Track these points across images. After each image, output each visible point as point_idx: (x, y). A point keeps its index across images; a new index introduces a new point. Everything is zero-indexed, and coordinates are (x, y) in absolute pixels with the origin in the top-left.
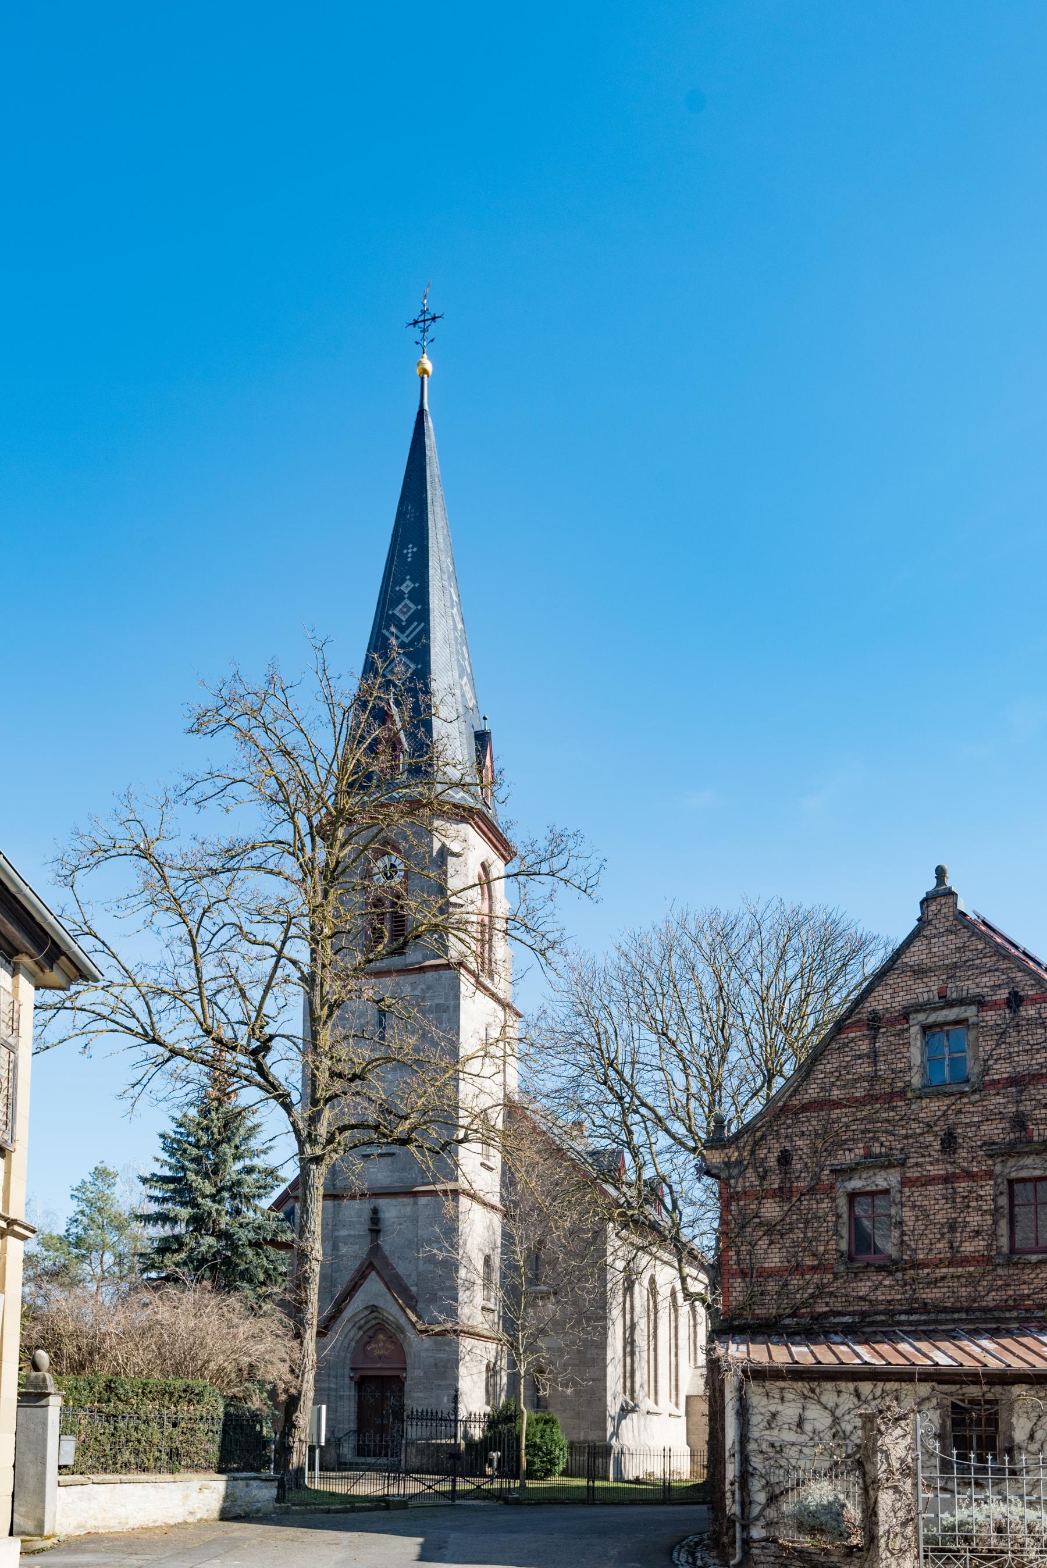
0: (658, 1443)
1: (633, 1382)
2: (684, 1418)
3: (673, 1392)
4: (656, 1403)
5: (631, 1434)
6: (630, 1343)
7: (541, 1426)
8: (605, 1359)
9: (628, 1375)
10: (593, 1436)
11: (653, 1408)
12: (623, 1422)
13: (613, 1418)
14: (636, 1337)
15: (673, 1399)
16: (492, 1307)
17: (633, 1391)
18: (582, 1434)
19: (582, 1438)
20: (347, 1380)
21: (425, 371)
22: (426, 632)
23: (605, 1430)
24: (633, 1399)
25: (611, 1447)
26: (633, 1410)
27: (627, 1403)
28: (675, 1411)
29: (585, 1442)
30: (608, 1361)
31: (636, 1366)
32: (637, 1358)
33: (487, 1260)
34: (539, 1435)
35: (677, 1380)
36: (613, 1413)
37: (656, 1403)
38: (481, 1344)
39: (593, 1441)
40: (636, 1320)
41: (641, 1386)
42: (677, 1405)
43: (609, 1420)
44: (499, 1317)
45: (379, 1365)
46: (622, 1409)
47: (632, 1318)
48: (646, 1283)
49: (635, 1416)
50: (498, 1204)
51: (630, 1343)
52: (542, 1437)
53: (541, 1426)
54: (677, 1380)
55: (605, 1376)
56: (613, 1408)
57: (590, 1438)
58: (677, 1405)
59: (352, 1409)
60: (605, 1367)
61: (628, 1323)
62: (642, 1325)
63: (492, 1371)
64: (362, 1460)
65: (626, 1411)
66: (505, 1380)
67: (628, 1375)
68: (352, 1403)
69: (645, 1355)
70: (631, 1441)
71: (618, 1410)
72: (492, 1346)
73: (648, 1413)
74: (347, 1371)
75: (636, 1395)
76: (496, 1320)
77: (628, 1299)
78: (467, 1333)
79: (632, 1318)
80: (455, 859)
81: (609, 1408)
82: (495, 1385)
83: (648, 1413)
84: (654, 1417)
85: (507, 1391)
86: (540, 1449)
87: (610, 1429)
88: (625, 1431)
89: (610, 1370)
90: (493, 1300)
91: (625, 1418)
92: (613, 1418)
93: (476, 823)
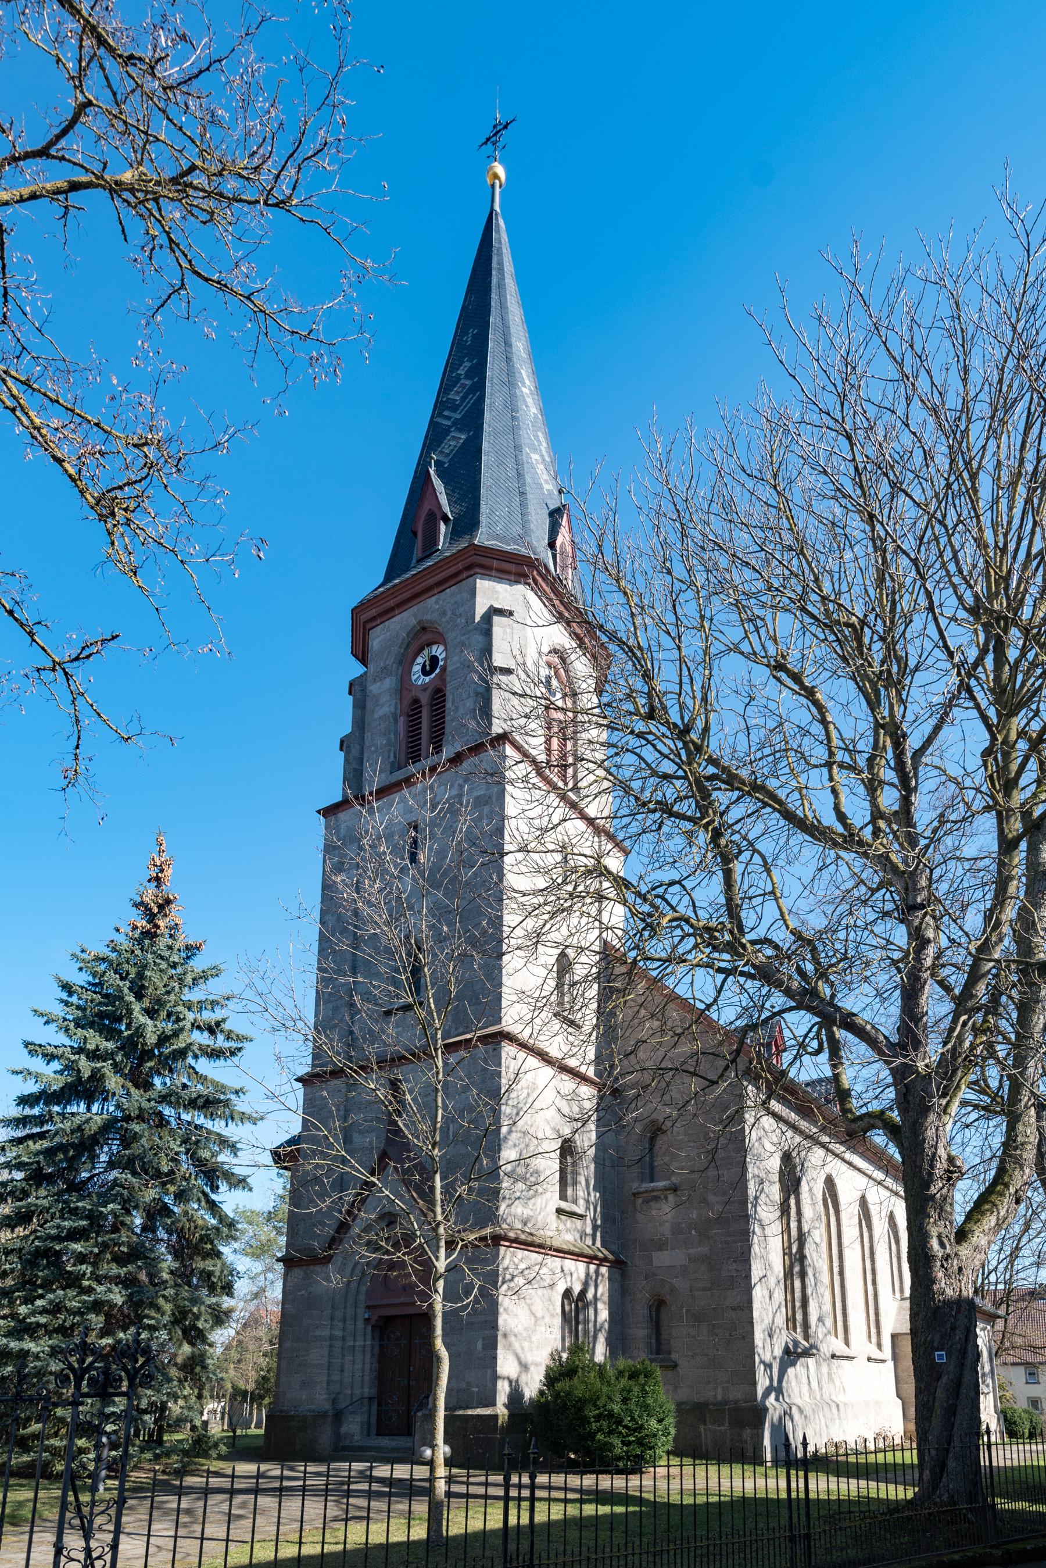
0: (851, 1400)
1: (805, 1314)
2: (890, 1364)
3: (873, 1330)
4: (847, 1343)
5: (805, 1389)
6: (796, 1262)
7: (624, 1382)
8: (748, 1277)
9: (798, 1304)
10: (736, 1394)
11: (836, 1345)
12: (791, 1371)
13: (768, 1366)
14: (807, 1252)
15: (874, 1339)
16: (580, 1210)
17: (806, 1326)
18: (720, 1391)
19: (719, 1398)
20: (360, 1324)
21: (496, 176)
22: (482, 399)
23: (754, 1383)
24: (806, 1337)
25: (766, 1409)
26: (806, 1353)
27: (796, 1343)
28: (876, 1354)
29: (725, 1402)
30: (754, 1279)
31: (809, 1291)
32: (810, 1280)
33: (567, 1149)
34: (618, 1398)
35: (877, 1314)
36: (767, 1358)
37: (847, 1343)
38: (554, 1263)
39: (736, 1402)
40: (805, 1229)
41: (820, 1319)
42: (879, 1346)
43: (760, 1370)
44: (595, 1228)
45: (402, 1300)
46: (787, 1351)
47: (800, 1228)
48: (819, 1187)
49: (811, 1361)
50: (591, 1072)
51: (796, 1262)
52: (625, 1401)
53: (624, 1382)
54: (877, 1314)
55: (750, 1301)
56: (767, 1348)
57: (731, 1397)
58: (879, 1346)
59: (367, 1366)
60: (749, 1289)
61: (794, 1232)
62: (817, 1236)
63: (575, 1306)
64: (385, 1442)
65: (791, 1356)
66: (604, 1315)
67: (798, 1304)
68: (368, 1356)
69: (825, 1278)
70: (806, 1398)
71: (778, 1352)
72: (579, 1269)
73: (833, 1356)
74: (361, 1310)
75: (812, 1331)
76: (589, 1230)
77: (792, 1201)
78: (516, 1241)
79: (800, 1228)
80: (504, 620)
81: (759, 1350)
82: (586, 1321)
83: (833, 1356)
84: (844, 1363)
85: (610, 1332)
86: (619, 1422)
87: (762, 1382)
88: (794, 1384)
89: (758, 1294)
90: (581, 1202)
91: (793, 1364)
92: (768, 1366)
93: (536, 582)
